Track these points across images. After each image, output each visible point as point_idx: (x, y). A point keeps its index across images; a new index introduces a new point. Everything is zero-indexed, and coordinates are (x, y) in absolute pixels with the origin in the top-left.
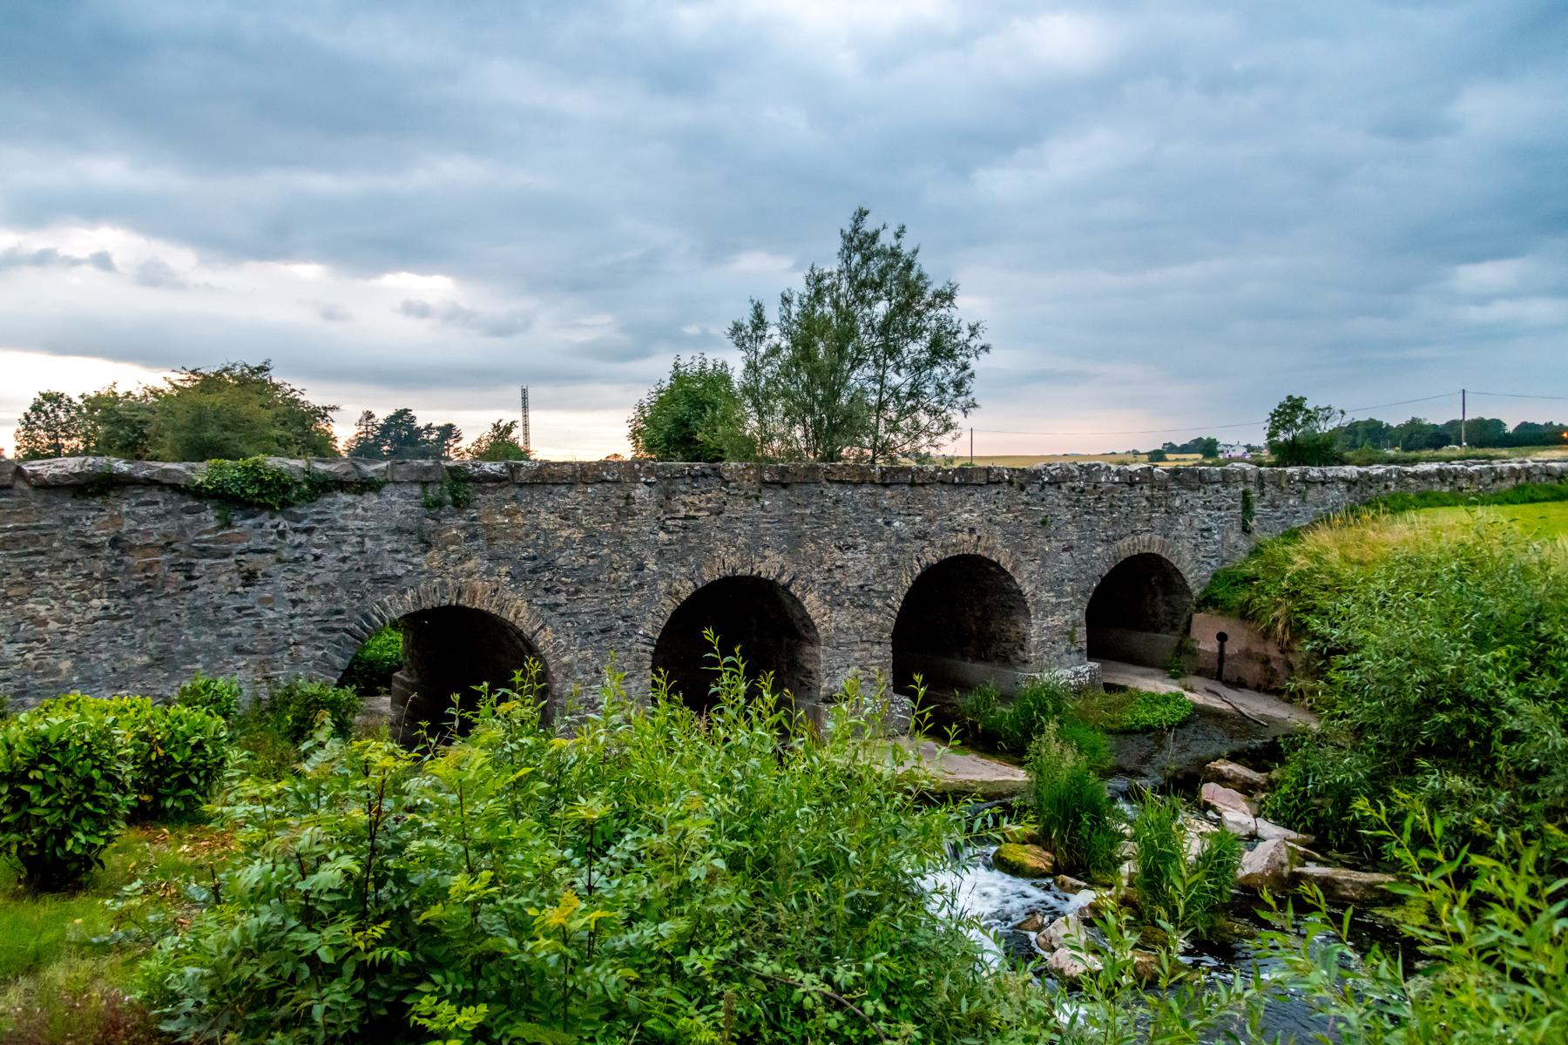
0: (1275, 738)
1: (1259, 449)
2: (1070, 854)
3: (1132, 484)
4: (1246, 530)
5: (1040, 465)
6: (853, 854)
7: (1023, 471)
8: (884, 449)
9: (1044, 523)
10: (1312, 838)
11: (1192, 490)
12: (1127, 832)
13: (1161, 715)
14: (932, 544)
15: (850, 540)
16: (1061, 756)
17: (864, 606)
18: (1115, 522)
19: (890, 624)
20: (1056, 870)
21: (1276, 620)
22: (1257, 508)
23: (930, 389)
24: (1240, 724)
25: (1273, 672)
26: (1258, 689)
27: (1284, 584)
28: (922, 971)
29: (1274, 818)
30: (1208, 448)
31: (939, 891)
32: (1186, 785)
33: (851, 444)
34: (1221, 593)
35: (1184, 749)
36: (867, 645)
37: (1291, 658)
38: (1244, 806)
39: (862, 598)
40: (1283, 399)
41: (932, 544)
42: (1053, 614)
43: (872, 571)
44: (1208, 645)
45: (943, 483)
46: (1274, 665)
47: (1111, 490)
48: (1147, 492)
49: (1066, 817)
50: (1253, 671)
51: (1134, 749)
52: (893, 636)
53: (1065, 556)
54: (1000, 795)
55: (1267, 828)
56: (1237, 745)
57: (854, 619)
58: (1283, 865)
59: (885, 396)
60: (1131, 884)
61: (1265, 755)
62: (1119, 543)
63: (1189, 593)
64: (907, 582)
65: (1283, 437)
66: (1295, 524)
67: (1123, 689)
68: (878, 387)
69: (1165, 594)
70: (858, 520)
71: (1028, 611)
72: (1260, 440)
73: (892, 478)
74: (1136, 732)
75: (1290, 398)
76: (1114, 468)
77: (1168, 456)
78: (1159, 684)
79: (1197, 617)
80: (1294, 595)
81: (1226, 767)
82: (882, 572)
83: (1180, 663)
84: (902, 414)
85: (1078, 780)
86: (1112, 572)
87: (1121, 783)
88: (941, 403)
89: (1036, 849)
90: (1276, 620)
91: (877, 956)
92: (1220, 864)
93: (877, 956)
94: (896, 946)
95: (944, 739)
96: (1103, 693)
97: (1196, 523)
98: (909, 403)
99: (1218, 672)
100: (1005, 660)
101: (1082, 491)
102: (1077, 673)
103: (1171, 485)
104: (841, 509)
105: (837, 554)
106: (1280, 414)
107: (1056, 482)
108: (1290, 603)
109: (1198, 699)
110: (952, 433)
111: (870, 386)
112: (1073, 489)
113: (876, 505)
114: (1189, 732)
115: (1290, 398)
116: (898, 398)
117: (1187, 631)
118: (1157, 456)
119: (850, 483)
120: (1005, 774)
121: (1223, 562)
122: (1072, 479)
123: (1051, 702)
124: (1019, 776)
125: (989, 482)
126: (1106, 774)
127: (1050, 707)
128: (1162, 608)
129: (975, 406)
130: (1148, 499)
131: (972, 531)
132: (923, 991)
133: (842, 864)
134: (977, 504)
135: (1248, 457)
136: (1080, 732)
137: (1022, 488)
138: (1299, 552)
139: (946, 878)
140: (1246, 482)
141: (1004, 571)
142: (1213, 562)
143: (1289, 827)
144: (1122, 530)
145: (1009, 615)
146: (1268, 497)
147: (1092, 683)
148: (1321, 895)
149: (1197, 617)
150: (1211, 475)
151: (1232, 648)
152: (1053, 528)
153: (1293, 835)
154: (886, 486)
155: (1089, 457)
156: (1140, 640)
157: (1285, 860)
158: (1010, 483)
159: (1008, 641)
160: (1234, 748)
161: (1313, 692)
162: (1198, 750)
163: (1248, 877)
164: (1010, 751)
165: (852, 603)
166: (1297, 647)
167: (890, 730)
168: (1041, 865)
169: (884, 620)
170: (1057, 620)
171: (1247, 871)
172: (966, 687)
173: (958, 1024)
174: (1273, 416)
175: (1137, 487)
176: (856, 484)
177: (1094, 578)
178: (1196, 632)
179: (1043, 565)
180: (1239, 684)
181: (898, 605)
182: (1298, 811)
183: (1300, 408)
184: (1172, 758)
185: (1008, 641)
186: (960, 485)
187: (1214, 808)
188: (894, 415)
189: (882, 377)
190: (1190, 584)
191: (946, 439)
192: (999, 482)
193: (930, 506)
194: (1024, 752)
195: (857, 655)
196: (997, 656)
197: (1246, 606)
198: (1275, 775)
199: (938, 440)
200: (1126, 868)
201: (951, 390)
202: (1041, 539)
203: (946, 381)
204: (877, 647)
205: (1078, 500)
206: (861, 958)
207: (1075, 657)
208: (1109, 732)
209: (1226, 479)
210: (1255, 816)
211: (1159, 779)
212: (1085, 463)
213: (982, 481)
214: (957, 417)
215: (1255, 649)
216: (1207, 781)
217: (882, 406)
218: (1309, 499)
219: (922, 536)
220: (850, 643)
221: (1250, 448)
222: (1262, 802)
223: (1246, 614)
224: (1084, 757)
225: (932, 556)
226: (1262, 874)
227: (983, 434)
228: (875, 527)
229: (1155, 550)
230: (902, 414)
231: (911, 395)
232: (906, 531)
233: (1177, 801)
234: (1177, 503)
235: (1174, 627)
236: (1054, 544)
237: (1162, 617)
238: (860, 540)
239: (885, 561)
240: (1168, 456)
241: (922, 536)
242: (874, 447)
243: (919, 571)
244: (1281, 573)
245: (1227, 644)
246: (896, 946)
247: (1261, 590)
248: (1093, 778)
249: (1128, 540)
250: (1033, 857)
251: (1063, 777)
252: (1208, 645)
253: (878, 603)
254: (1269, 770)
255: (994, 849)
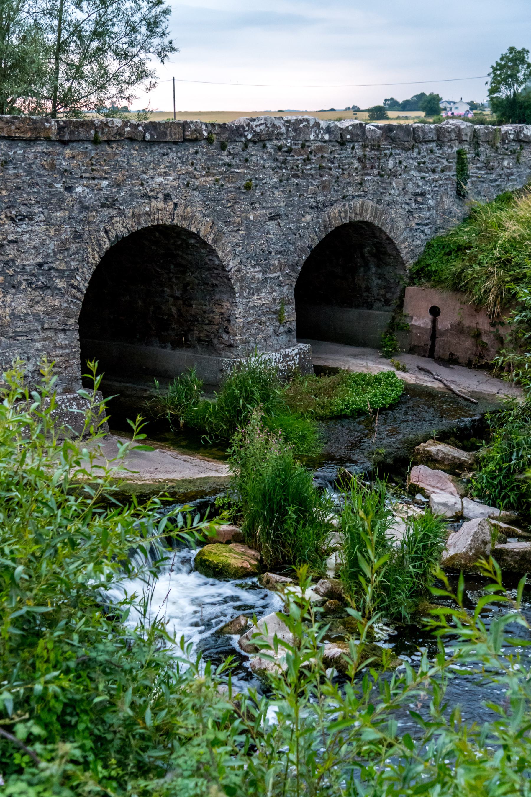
0: (483, 415)
1: (482, 107)
2: (275, 550)
3: (342, 143)
4: (460, 194)
5: (242, 120)
6: (20, 569)
7: (223, 127)
8: (67, 99)
9: (248, 187)
10: (514, 515)
11: (406, 149)
12: (335, 522)
13: (365, 399)
14: (121, 213)
15: (23, 209)
16: (266, 448)
17: (44, 287)
18: (325, 187)
19: (76, 308)
20: (262, 567)
21: (487, 292)
22: (472, 169)
23: (119, 27)
24: (451, 402)
25: (484, 346)
26: (469, 365)
27: (496, 253)
28: (101, 687)
29: (480, 497)
30: (430, 104)
31: (130, 600)
32: (394, 471)
33: (26, 93)
34: (434, 264)
35: (394, 432)
36: (50, 334)
37: (502, 331)
38: (451, 487)
39: (41, 278)
40: (505, 51)
41: (121, 213)
42: (259, 291)
43: (53, 245)
44: (421, 321)
45: (131, 140)
46: (485, 339)
47: (320, 149)
48: (359, 152)
49: (271, 511)
50: (465, 347)
51: (344, 434)
52: (81, 321)
53: (272, 225)
54: (203, 494)
55: (475, 509)
56: (446, 424)
57: (34, 303)
58: (485, 543)
59: (65, 35)
60: (337, 576)
61: (471, 435)
62: (329, 210)
63: (403, 263)
64: (95, 258)
65: (505, 93)
66: (509, 187)
67: (334, 371)
68: (56, 22)
69: (378, 266)
70: (32, 185)
71: (232, 288)
72: (482, 97)
73: (74, 133)
74: (346, 416)
75: (512, 49)
76: (323, 124)
77: (390, 114)
78: (370, 364)
79: (411, 290)
80: (505, 263)
81: (435, 448)
82: (63, 248)
83: (391, 341)
84: (85, 56)
85: (283, 471)
86: (322, 242)
87: (330, 472)
88: (132, 44)
89: (239, 548)
90: (487, 292)
91: (48, 677)
92: (425, 547)
93: (48, 677)
94: (72, 664)
95: (128, 432)
96: (314, 377)
97: (410, 187)
98: (95, 44)
99: (431, 349)
100: (209, 345)
101: (289, 151)
102: (285, 356)
103: (385, 144)
104: (12, 171)
105: (8, 226)
106: (502, 67)
107: (260, 140)
108: (501, 272)
109: (410, 378)
110: (146, 82)
111: (45, 21)
112: (280, 148)
113: (53, 167)
114: (399, 414)
115: (512, 49)
116: (80, 37)
117: (401, 306)
118: (377, 113)
119: (20, 139)
120: (208, 469)
121: (437, 229)
122: (279, 136)
123: (259, 388)
124: (222, 471)
125: (185, 140)
126: (312, 464)
127: (257, 395)
128: (376, 282)
129: (173, 49)
130: (359, 160)
131: (167, 197)
132: (103, 708)
133: (8, 581)
134: (172, 166)
135: (470, 116)
136: (291, 421)
137: (223, 147)
138: (511, 218)
139: (134, 587)
140: (461, 141)
141: (205, 244)
142: (427, 230)
143: (494, 505)
144: (332, 195)
145: (211, 293)
146: (482, 158)
147: (303, 368)
148: (497, 566)
149: (411, 290)
150: (425, 133)
151: (444, 324)
152: (258, 193)
153: (497, 512)
154: (65, 143)
155: (306, 112)
156: (352, 317)
157: (488, 538)
158: (209, 140)
159: (210, 323)
160: (442, 428)
161: (520, 365)
162: (407, 432)
163: (452, 558)
164: (215, 445)
165: (30, 284)
166: (506, 319)
167: (70, 429)
168: (246, 564)
169: (66, 301)
170: (264, 298)
171: (452, 552)
172: (167, 377)
173: (142, 737)
174: (495, 69)
175: (349, 147)
176: (30, 142)
177: (303, 250)
178: (408, 309)
179: (248, 236)
180: (451, 361)
181: (84, 286)
182: (503, 488)
183: (523, 61)
184: (382, 442)
185: (210, 323)
186: (152, 143)
187: (421, 491)
188: (75, 58)
189: (60, 11)
190: (404, 254)
191: (138, 90)
192: (195, 141)
193: (117, 168)
194: (228, 445)
195: (38, 345)
196: (199, 340)
197: (458, 276)
198: (483, 453)
199: (129, 91)
200: (332, 561)
201: (143, 29)
202: (245, 205)
203: (136, 18)
204: (61, 335)
205: (285, 162)
206: (33, 680)
207: (283, 338)
208: (320, 418)
209: (441, 137)
210: (462, 496)
211: (369, 465)
212: (293, 118)
213: (177, 138)
214: (152, 63)
215: (467, 322)
216: (416, 463)
217: (61, 47)
218: (522, 160)
219: (110, 203)
220: (30, 331)
221: (473, 106)
222: (469, 481)
223: (458, 286)
224: (290, 446)
225: (122, 227)
226: (466, 553)
227: (184, 85)
228: (54, 194)
229: (368, 218)
230: (85, 56)
231: (96, 35)
232: (91, 199)
233: (381, 486)
234: (391, 164)
235: (387, 302)
236: (260, 212)
237: (375, 291)
238: (36, 209)
239: (67, 233)
240: (390, 114)
241: (110, 203)
242: (54, 98)
243: (107, 245)
244: (493, 239)
245: (439, 318)
246: (72, 664)
247: (473, 260)
248: (299, 467)
249: (339, 207)
250: (236, 557)
251: (268, 470)
252: (421, 321)
253: (61, 284)
254: (477, 448)
255: (194, 552)
